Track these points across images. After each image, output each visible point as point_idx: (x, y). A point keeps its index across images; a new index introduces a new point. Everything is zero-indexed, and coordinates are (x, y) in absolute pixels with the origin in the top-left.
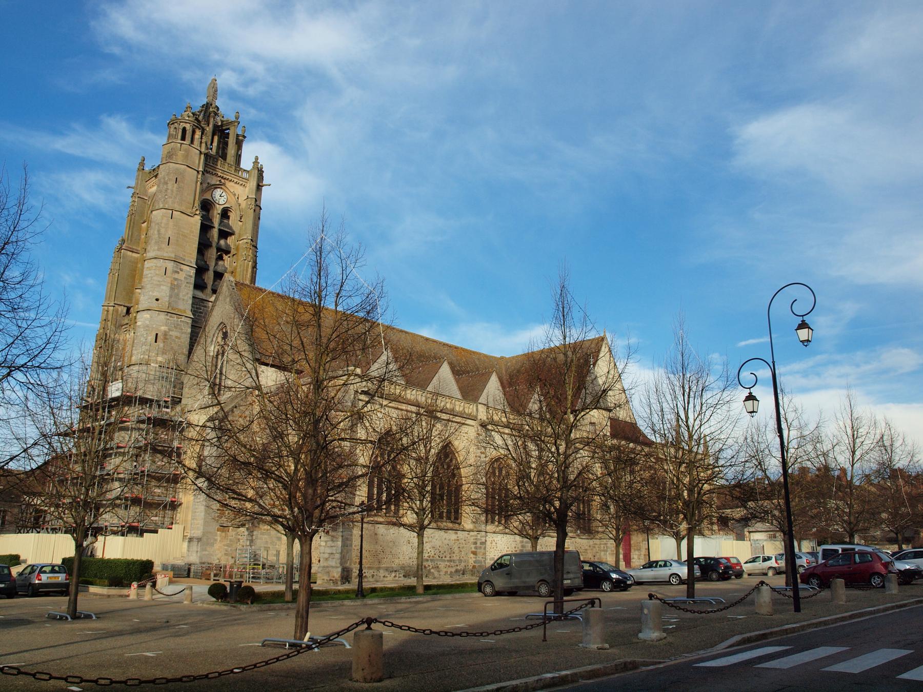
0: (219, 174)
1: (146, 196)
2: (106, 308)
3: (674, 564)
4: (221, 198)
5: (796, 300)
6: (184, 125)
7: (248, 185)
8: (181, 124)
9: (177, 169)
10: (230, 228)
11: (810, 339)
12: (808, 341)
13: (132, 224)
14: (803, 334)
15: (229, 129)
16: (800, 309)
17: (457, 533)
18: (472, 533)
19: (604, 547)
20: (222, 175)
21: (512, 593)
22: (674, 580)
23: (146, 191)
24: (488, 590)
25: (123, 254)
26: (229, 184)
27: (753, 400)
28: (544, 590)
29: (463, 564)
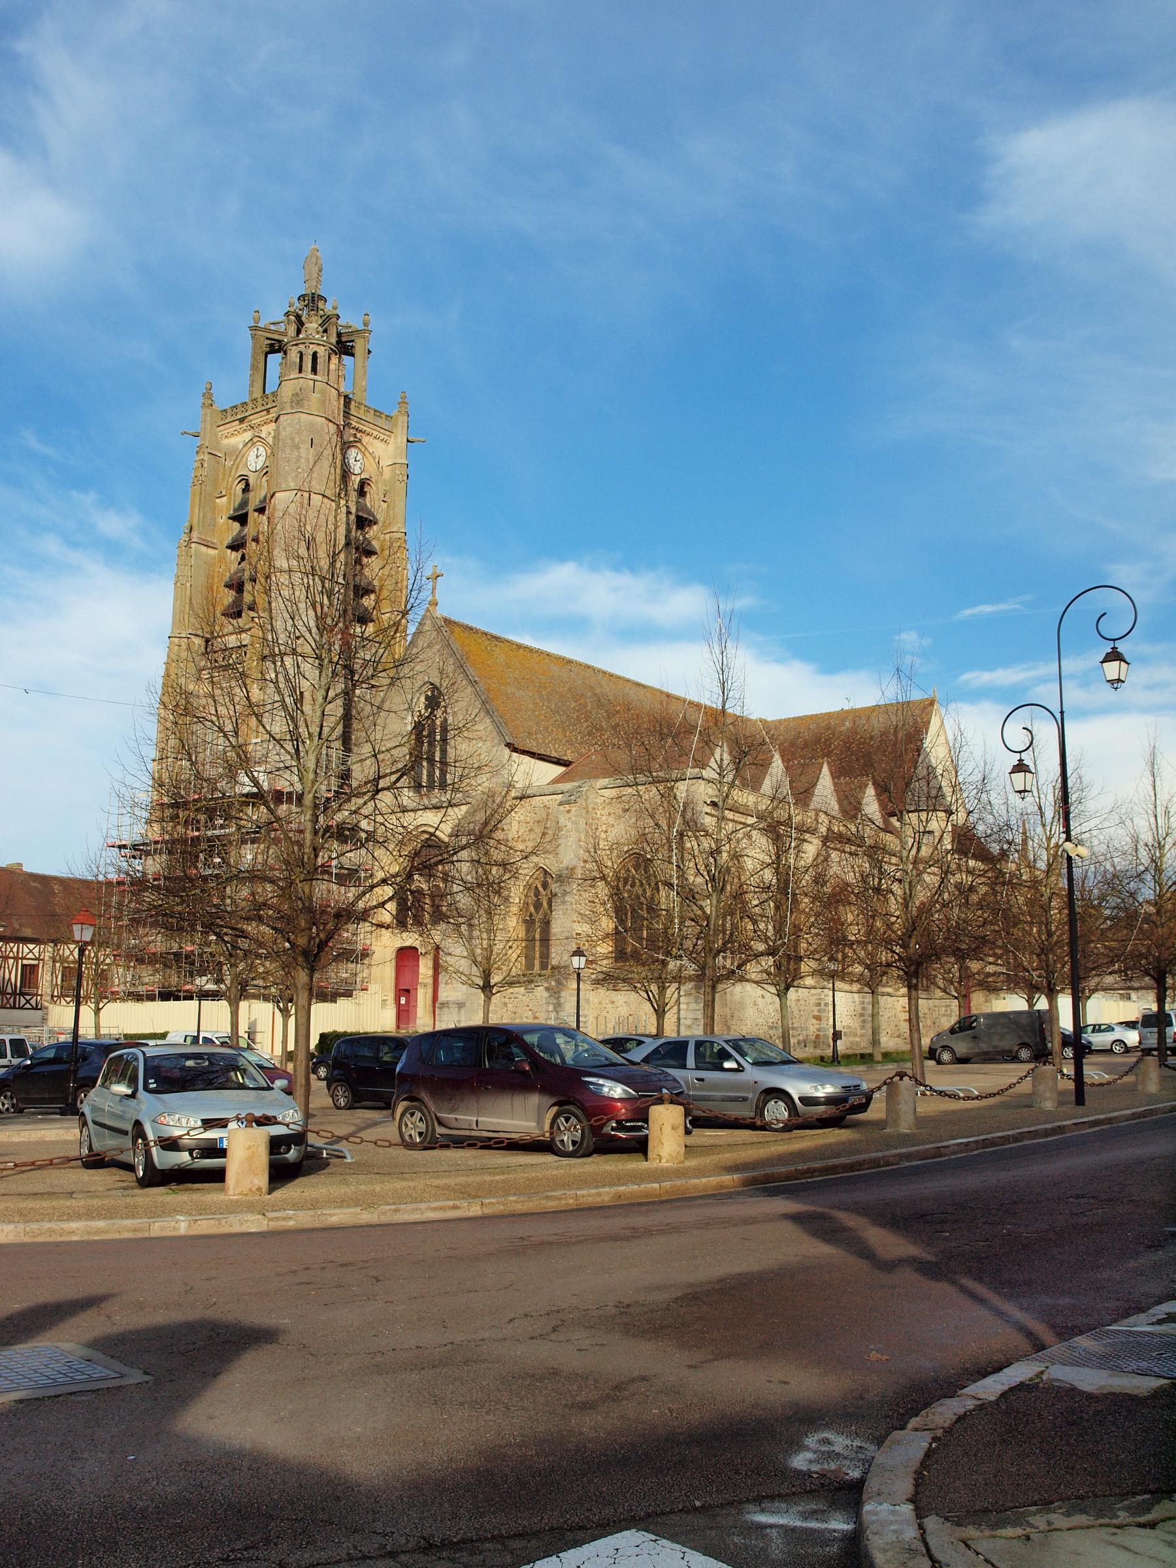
0: (354, 424)
1: (220, 451)
2: (176, 640)
3: (1117, 1028)
4: (357, 462)
5: (1105, 614)
6: (313, 348)
7: (392, 441)
8: (311, 346)
9: (312, 424)
10: (370, 513)
11: (1122, 678)
12: (1119, 680)
13: (203, 499)
14: (1112, 669)
15: (353, 341)
16: (1112, 628)
17: (797, 991)
18: (813, 991)
19: (946, 1011)
20: (357, 425)
21: (988, 1058)
22: (1117, 1049)
23: (218, 442)
24: (946, 1056)
25: (196, 551)
26: (366, 440)
27: (1025, 771)
28: (1024, 1054)
29: (804, 1033)
